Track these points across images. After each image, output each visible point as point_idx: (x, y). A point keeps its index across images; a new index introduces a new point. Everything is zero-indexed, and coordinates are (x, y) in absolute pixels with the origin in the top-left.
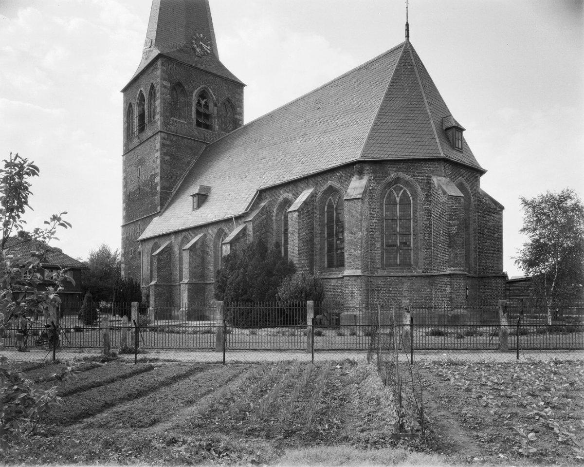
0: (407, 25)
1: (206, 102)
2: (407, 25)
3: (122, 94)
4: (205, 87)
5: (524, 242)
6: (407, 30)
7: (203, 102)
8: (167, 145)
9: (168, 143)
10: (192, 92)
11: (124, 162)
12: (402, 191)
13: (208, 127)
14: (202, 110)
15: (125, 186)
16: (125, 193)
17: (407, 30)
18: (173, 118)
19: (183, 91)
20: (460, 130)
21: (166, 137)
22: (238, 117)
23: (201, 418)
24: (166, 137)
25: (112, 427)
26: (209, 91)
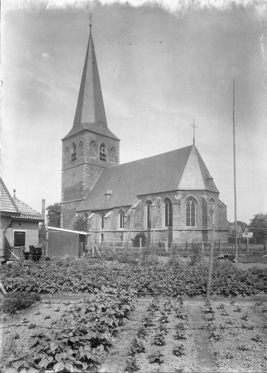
0: (194, 138)
1: (104, 149)
2: (194, 138)
3: (62, 141)
4: (103, 142)
5: (32, 244)
6: (194, 140)
7: (102, 149)
8: (88, 169)
9: (88, 168)
10: (98, 145)
11: (63, 174)
12: (203, 245)
13: (104, 160)
14: (102, 152)
15: (63, 184)
16: (62, 188)
17: (194, 140)
18: (90, 157)
19: (95, 145)
20: (212, 179)
21: (88, 165)
22: (117, 155)
23: (5, 356)
24: (88, 165)
25: (33, 307)
26: (105, 143)
